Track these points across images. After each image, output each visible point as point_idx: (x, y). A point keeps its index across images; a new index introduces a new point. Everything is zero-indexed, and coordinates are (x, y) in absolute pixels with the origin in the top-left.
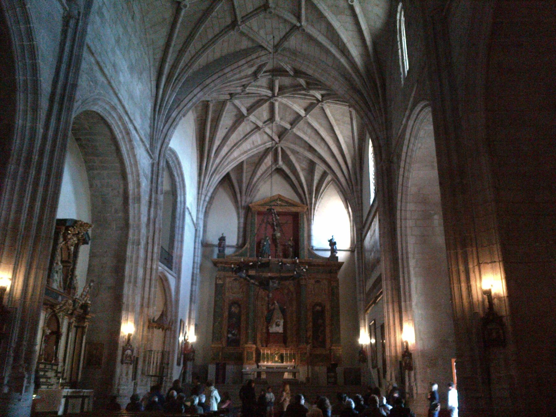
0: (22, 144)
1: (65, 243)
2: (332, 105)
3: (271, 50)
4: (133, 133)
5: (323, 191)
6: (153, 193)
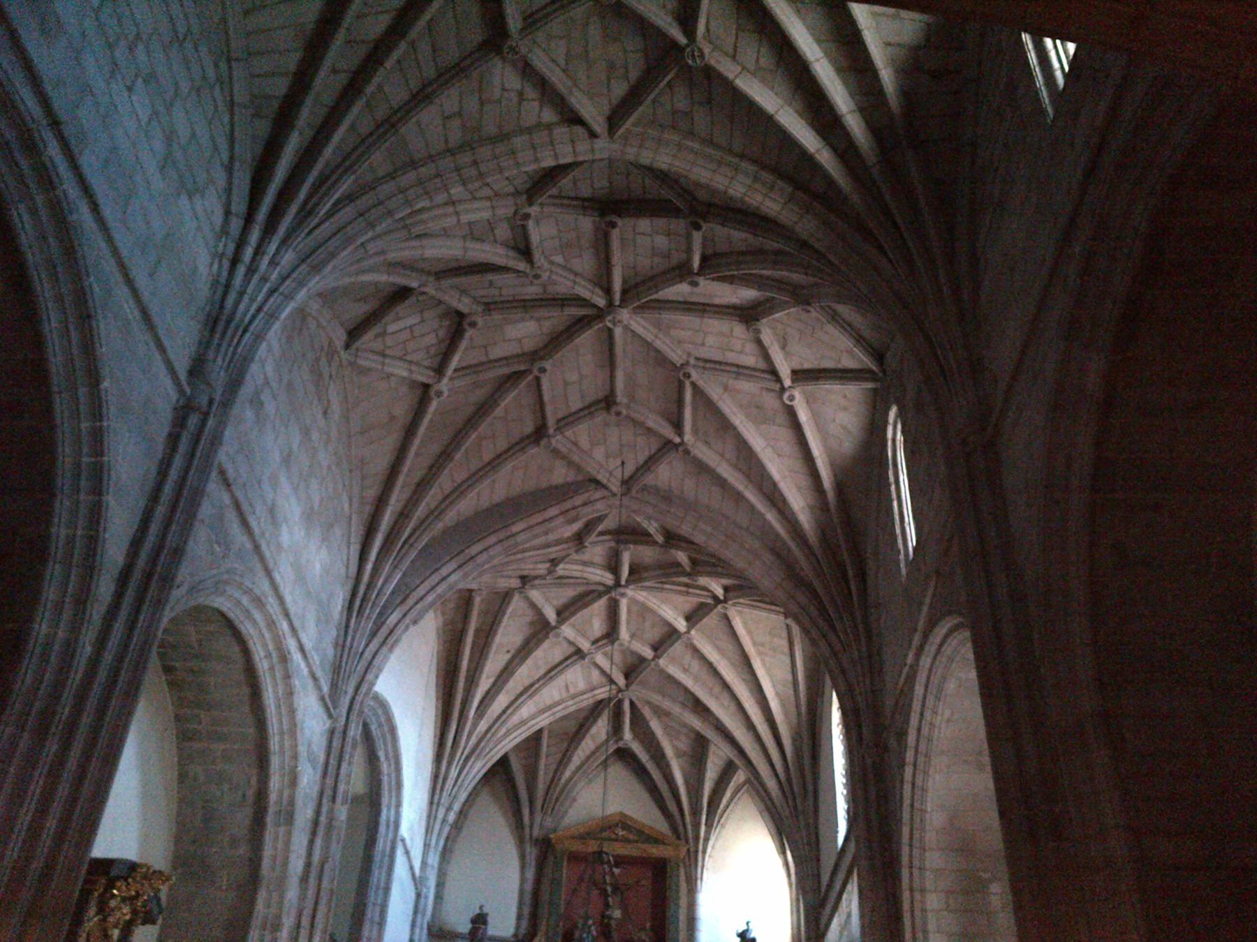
0: (39, 681)
1: (100, 920)
2: (746, 610)
3: (614, 489)
4: (295, 658)
5: (727, 807)
6: (325, 801)
